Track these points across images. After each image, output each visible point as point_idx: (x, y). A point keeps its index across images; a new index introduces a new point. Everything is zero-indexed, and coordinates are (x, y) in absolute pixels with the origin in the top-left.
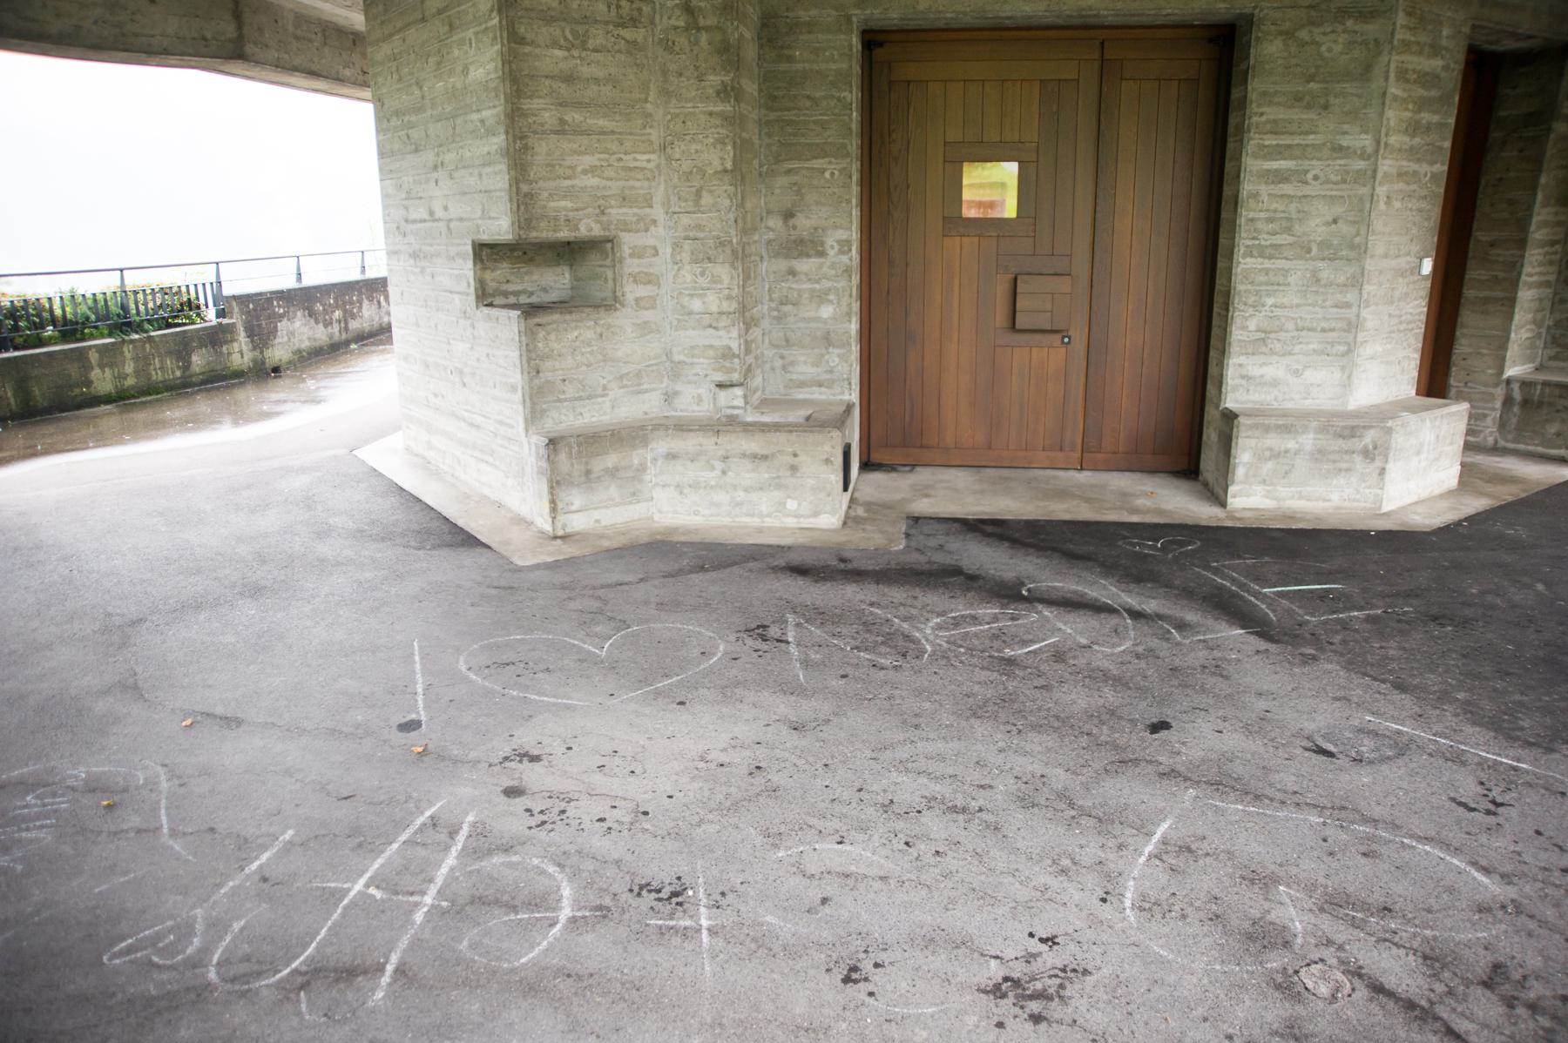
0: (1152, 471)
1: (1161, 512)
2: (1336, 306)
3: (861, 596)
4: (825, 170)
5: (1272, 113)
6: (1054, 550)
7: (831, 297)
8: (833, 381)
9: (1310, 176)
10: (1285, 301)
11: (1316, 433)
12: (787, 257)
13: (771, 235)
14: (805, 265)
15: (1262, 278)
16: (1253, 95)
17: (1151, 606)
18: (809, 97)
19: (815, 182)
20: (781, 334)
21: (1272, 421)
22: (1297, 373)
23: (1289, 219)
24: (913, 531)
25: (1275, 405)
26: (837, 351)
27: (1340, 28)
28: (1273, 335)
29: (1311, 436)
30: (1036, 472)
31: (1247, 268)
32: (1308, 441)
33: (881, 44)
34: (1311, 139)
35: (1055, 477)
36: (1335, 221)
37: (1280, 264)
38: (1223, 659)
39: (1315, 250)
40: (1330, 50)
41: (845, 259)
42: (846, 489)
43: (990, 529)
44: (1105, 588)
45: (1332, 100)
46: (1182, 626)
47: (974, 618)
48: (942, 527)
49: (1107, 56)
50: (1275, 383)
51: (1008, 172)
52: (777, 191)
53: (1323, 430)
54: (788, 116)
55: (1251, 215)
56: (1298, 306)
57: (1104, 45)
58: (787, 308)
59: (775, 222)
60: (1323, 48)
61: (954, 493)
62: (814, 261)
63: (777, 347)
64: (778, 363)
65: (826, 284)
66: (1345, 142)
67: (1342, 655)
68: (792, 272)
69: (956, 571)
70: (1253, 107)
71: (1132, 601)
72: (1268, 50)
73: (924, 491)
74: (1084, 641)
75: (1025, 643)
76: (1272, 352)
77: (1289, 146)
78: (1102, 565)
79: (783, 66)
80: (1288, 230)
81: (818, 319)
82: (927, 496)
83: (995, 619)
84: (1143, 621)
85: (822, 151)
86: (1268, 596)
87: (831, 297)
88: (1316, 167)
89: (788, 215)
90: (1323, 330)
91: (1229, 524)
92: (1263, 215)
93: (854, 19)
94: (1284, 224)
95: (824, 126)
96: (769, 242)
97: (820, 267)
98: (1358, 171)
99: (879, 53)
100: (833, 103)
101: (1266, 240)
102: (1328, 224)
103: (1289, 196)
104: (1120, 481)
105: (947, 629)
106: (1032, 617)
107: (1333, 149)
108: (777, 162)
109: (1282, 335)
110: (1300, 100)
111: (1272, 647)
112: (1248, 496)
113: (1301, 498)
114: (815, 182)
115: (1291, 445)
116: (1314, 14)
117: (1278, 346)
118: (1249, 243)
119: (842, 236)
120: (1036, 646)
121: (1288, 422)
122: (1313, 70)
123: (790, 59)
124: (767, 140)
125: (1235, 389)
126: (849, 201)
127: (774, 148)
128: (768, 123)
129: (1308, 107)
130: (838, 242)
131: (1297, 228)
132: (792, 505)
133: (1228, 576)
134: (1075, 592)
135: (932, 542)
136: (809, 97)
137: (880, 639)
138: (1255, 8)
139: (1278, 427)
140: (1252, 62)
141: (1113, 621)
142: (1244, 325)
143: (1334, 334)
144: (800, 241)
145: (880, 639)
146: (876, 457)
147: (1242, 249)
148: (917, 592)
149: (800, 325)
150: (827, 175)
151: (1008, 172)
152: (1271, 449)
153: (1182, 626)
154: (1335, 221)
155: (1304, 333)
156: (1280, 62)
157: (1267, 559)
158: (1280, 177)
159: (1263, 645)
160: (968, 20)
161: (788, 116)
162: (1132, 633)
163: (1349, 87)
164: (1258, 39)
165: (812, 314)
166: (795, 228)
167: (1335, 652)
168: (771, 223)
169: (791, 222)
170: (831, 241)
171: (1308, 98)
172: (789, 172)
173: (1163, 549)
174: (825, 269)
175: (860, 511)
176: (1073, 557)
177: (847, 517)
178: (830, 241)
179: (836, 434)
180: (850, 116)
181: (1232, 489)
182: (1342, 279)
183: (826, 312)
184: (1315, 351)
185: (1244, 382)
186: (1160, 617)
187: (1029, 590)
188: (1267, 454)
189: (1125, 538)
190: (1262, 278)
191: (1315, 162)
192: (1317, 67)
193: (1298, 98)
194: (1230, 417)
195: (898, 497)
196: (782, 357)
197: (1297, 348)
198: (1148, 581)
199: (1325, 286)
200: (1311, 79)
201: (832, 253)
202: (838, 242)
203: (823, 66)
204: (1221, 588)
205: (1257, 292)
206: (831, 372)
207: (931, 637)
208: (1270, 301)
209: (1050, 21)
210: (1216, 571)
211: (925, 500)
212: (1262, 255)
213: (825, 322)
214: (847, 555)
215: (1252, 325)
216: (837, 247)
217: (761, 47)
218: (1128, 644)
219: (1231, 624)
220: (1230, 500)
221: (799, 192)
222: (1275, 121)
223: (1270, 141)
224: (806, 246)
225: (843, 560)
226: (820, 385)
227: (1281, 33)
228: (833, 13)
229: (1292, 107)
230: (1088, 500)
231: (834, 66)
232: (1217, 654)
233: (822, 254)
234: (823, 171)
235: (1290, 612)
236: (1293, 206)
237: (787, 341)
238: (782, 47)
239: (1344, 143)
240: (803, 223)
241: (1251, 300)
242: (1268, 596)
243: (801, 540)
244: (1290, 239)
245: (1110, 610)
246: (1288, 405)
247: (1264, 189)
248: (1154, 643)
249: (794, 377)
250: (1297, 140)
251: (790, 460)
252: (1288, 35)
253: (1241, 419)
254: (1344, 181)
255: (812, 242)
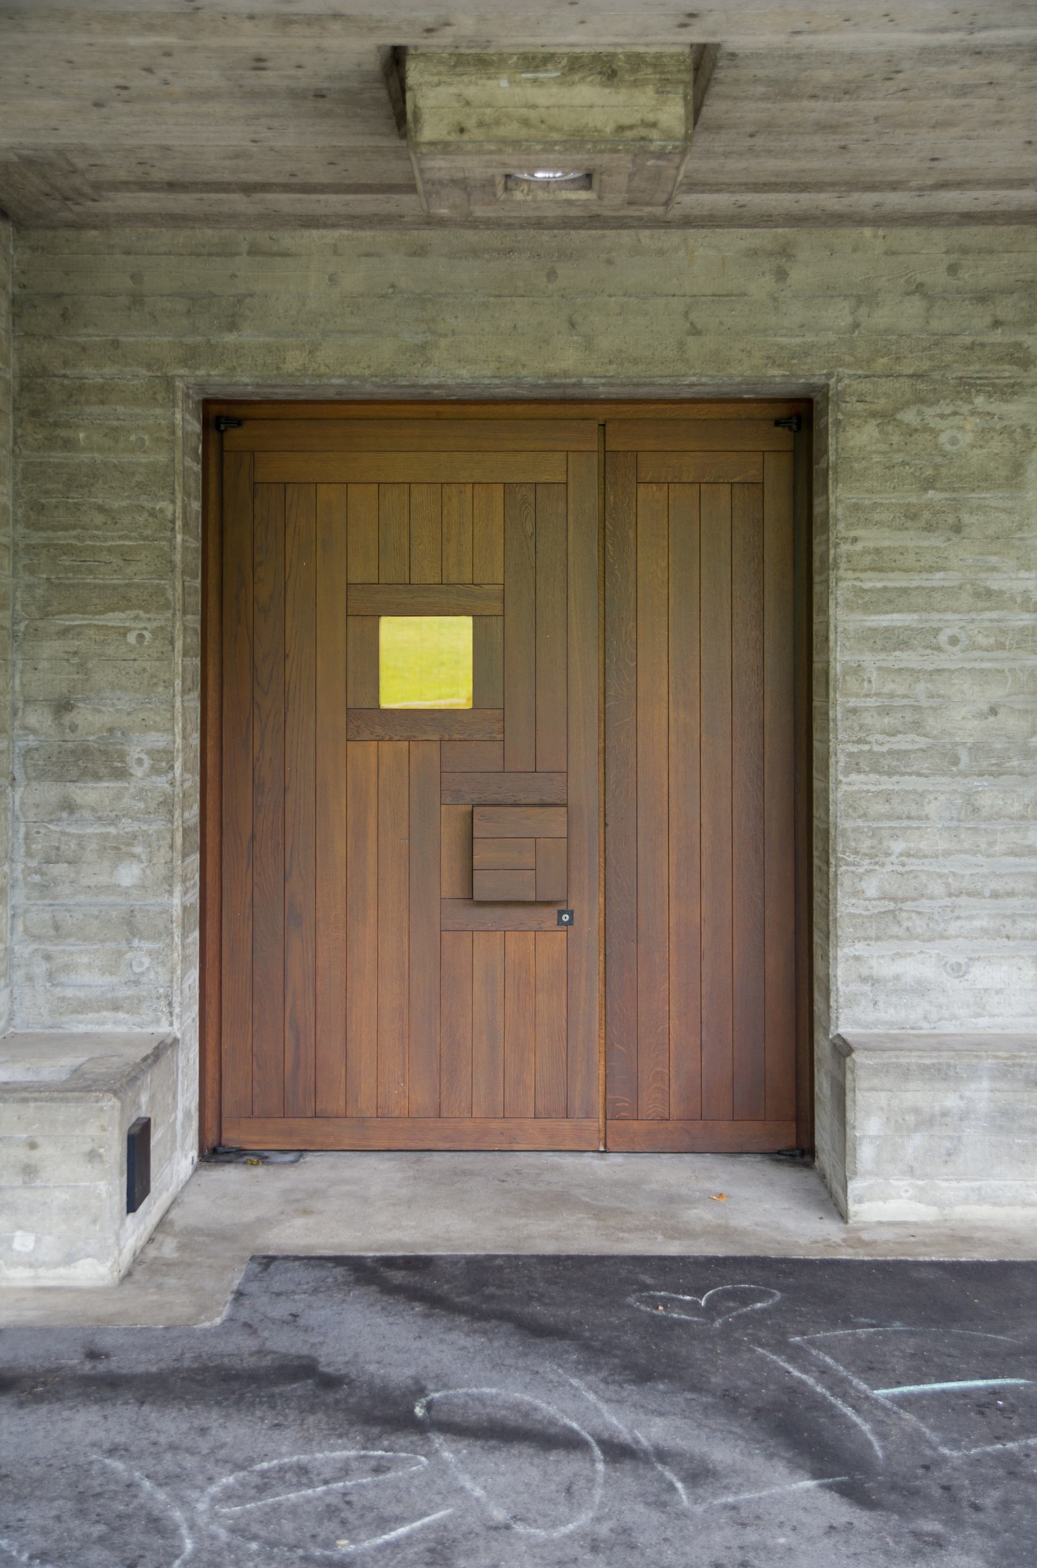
0: (735, 1151)
1: (726, 1233)
2: (1013, 853)
3: (97, 1434)
4: (128, 630)
5: (870, 538)
6: (503, 1316)
7: (138, 850)
8: (140, 1000)
9: (943, 638)
10: (923, 845)
11: (993, 1078)
12: (60, 778)
13: (32, 741)
14: (89, 794)
15: (882, 808)
16: (837, 510)
17: (650, 1430)
18: (101, 509)
19: (110, 651)
20: (47, 916)
21: (912, 1059)
22: (958, 971)
23: (917, 709)
24: (253, 1287)
25: (926, 1028)
26: (147, 945)
27: (966, 408)
28: (908, 905)
29: (985, 1084)
30: (523, 1158)
31: (850, 788)
32: (980, 1093)
33: (239, 422)
34: (938, 579)
35: (555, 1168)
36: (993, 711)
37: (909, 783)
38: (762, 1548)
39: (964, 758)
40: (954, 441)
41: (161, 782)
42: (133, 1201)
43: (398, 1277)
44: (576, 1396)
45: (966, 518)
46: (699, 1474)
47: (302, 1470)
48: (309, 1276)
49: (612, 446)
50: (921, 989)
51: (455, 635)
52: (44, 665)
53: (1004, 1072)
54: (63, 538)
55: (853, 702)
56: (947, 853)
57: (615, 429)
58: (58, 869)
59: (38, 718)
60: (943, 438)
61: (362, 1202)
62: (108, 786)
63: (38, 938)
64: (40, 968)
65: (128, 826)
66: (995, 582)
67: (993, 1534)
68: (69, 806)
69: (303, 1370)
70: (840, 529)
71: (618, 1421)
72: (852, 440)
73: (301, 1204)
74: (499, 1515)
75: (384, 1523)
76: (911, 935)
77: (904, 591)
78: (586, 1346)
79: (57, 456)
80: (917, 726)
81: (113, 888)
82: (306, 1212)
83: (345, 1470)
84: (628, 1465)
85: (122, 599)
86: (883, 1406)
87: (138, 850)
88: (952, 623)
89: (63, 706)
90: (995, 895)
91: (845, 1254)
92: (871, 702)
93: (179, 384)
94: (909, 716)
95: (126, 556)
96: (28, 752)
97: (119, 796)
98: (1022, 630)
99: (236, 437)
100: (141, 519)
101: (880, 744)
102: (982, 716)
103: (912, 671)
104: (670, 1172)
105: (242, 1499)
106: (413, 1463)
107: (977, 595)
108: (45, 615)
109: (924, 905)
110: (915, 517)
111: (861, 1518)
112: (885, 1199)
113: (981, 1199)
114: (110, 651)
115: (951, 1101)
116: (921, 386)
117: (919, 925)
118: (854, 749)
119: (160, 736)
120: (402, 1531)
121: (942, 1059)
122: (929, 472)
123: (68, 444)
124: (28, 578)
125: (851, 1001)
126: (169, 684)
127: (39, 592)
128: (29, 548)
129: (929, 528)
130: (149, 752)
131: (931, 722)
132: (23, 1242)
133: (813, 1365)
134: (516, 1407)
135: (281, 1309)
136: (101, 509)
137: (100, 1529)
138: (829, 375)
139: (924, 1069)
140: (832, 458)
141: (567, 1466)
142: (856, 890)
143: (1014, 902)
144: (84, 752)
145: (100, 1529)
146: (233, 1137)
147: (842, 759)
148: (213, 1418)
149: (81, 898)
150: (131, 638)
151: (455, 635)
152: (916, 1111)
153: (699, 1474)
154: (993, 711)
155: (963, 900)
156: (876, 458)
157: (898, 1325)
158: (895, 640)
159: (842, 1511)
160: (368, 389)
161: (63, 538)
162: (598, 1493)
163: (991, 498)
164: (838, 423)
165: (104, 879)
166: (73, 728)
167: (981, 1527)
168: (32, 719)
169: (67, 719)
170: (137, 751)
171: (926, 515)
172: (64, 632)
173: (712, 1310)
174: (126, 800)
175: (169, 1248)
176: (536, 1331)
177: (137, 1260)
178: (134, 752)
179: (110, 1103)
180: (171, 540)
181: (855, 1186)
182: (1016, 808)
183: (128, 874)
184: (985, 931)
185: (867, 988)
186: (663, 1455)
187: (429, 1407)
188: (911, 1119)
189: (646, 1287)
190: (882, 808)
191: (949, 616)
192: (936, 467)
193: (911, 514)
194: (843, 1049)
195: (250, 1215)
196: (48, 957)
197: (954, 927)
198: (662, 1377)
199: (989, 819)
200: (929, 484)
201: (138, 772)
202: (149, 752)
203: (126, 458)
204: (796, 1389)
205: (875, 833)
206: (137, 983)
207: (202, 1520)
208: (898, 847)
209: (506, 391)
210: (795, 1354)
211: (300, 1221)
212: (875, 770)
213: (126, 892)
214: (106, 1342)
215: (871, 887)
216: (147, 762)
217: (19, 423)
218: (583, 1519)
219: (794, 1467)
220: (853, 1208)
221: (82, 667)
222: (878, 551)
223: (872, 582)
224: (97, 760)
225: (93, 1355)
226: (116, 1008)
227: (874, 414)
228: (143, 372)
229: (902, 528)
230: (599, 1213)
231: (143, 459)
232: (751, 1536)
233: (121, 774)
234: (124, 632)
235: (915, 1439)
236: (921, 687)
237: (57, 928)
238: (56, 425)
239: (995, 586)
240: (90, 721)
241: (866, 845)
242: (883, 1406)
243: (30, 1314)
244: (923, 742)
245: (570, 1442)
246: (949, 1028)
247: (869, 660)
248: (637, 1513)
249: (69, 992)
250: (916, 581)
251: (22, 1154)
252: (886, 417)
253: (858, 1057)
254: (1001, 646)
255: (105, 753)
